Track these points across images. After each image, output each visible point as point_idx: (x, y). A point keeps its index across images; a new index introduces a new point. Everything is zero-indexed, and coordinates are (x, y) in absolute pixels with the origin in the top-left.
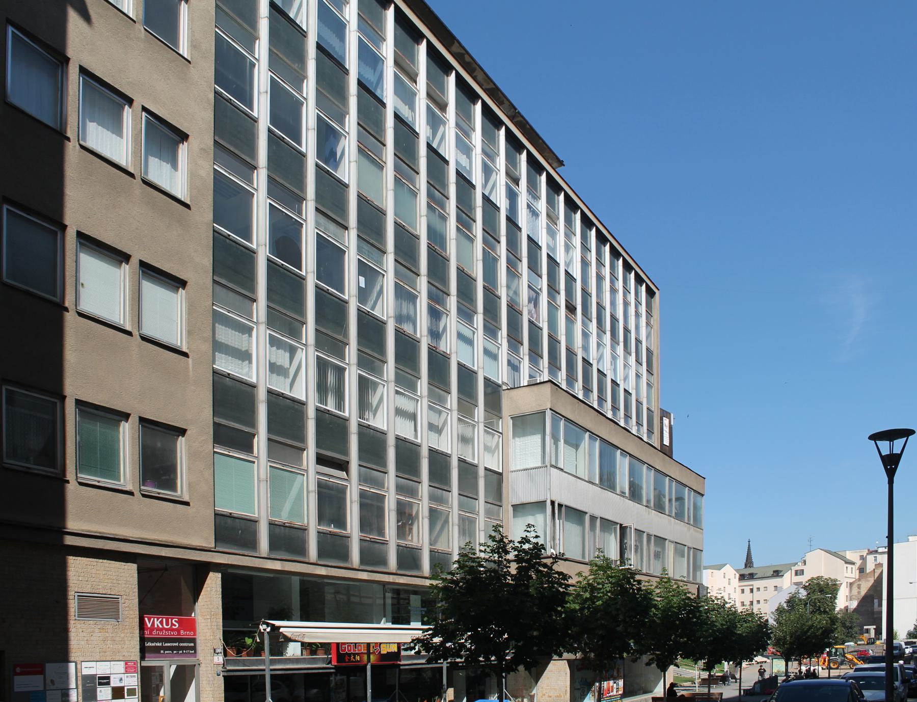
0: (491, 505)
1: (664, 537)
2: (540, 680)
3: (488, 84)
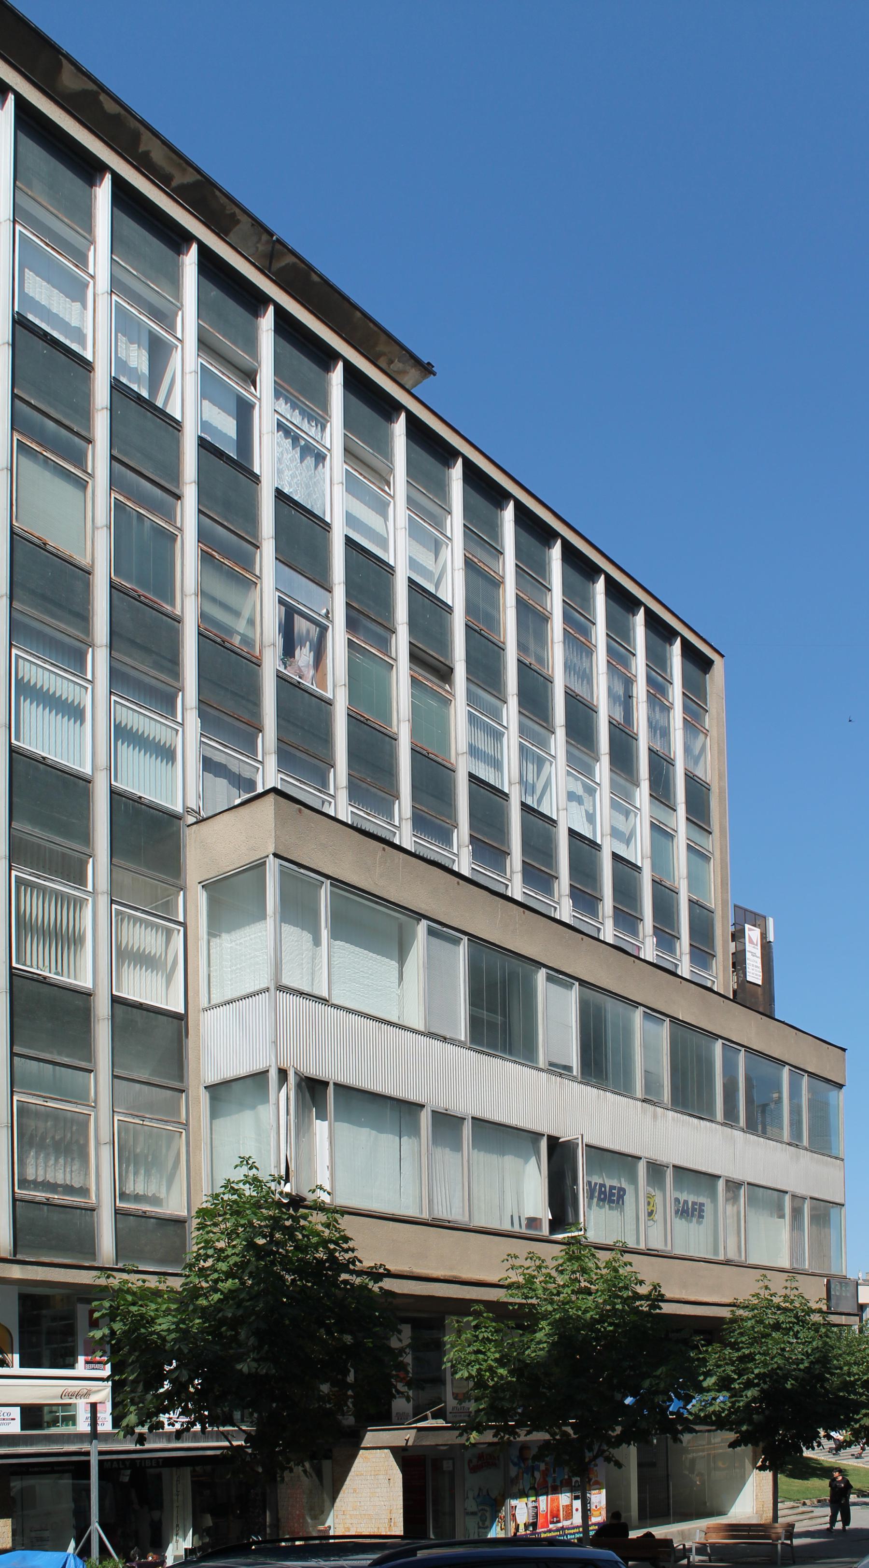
0: (146, 1088)
1: (710, 1170)
2: (340, 1496)
3: (184, 171)
